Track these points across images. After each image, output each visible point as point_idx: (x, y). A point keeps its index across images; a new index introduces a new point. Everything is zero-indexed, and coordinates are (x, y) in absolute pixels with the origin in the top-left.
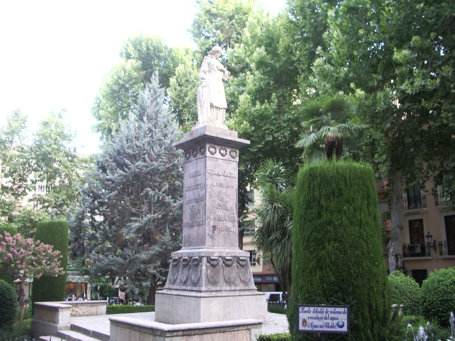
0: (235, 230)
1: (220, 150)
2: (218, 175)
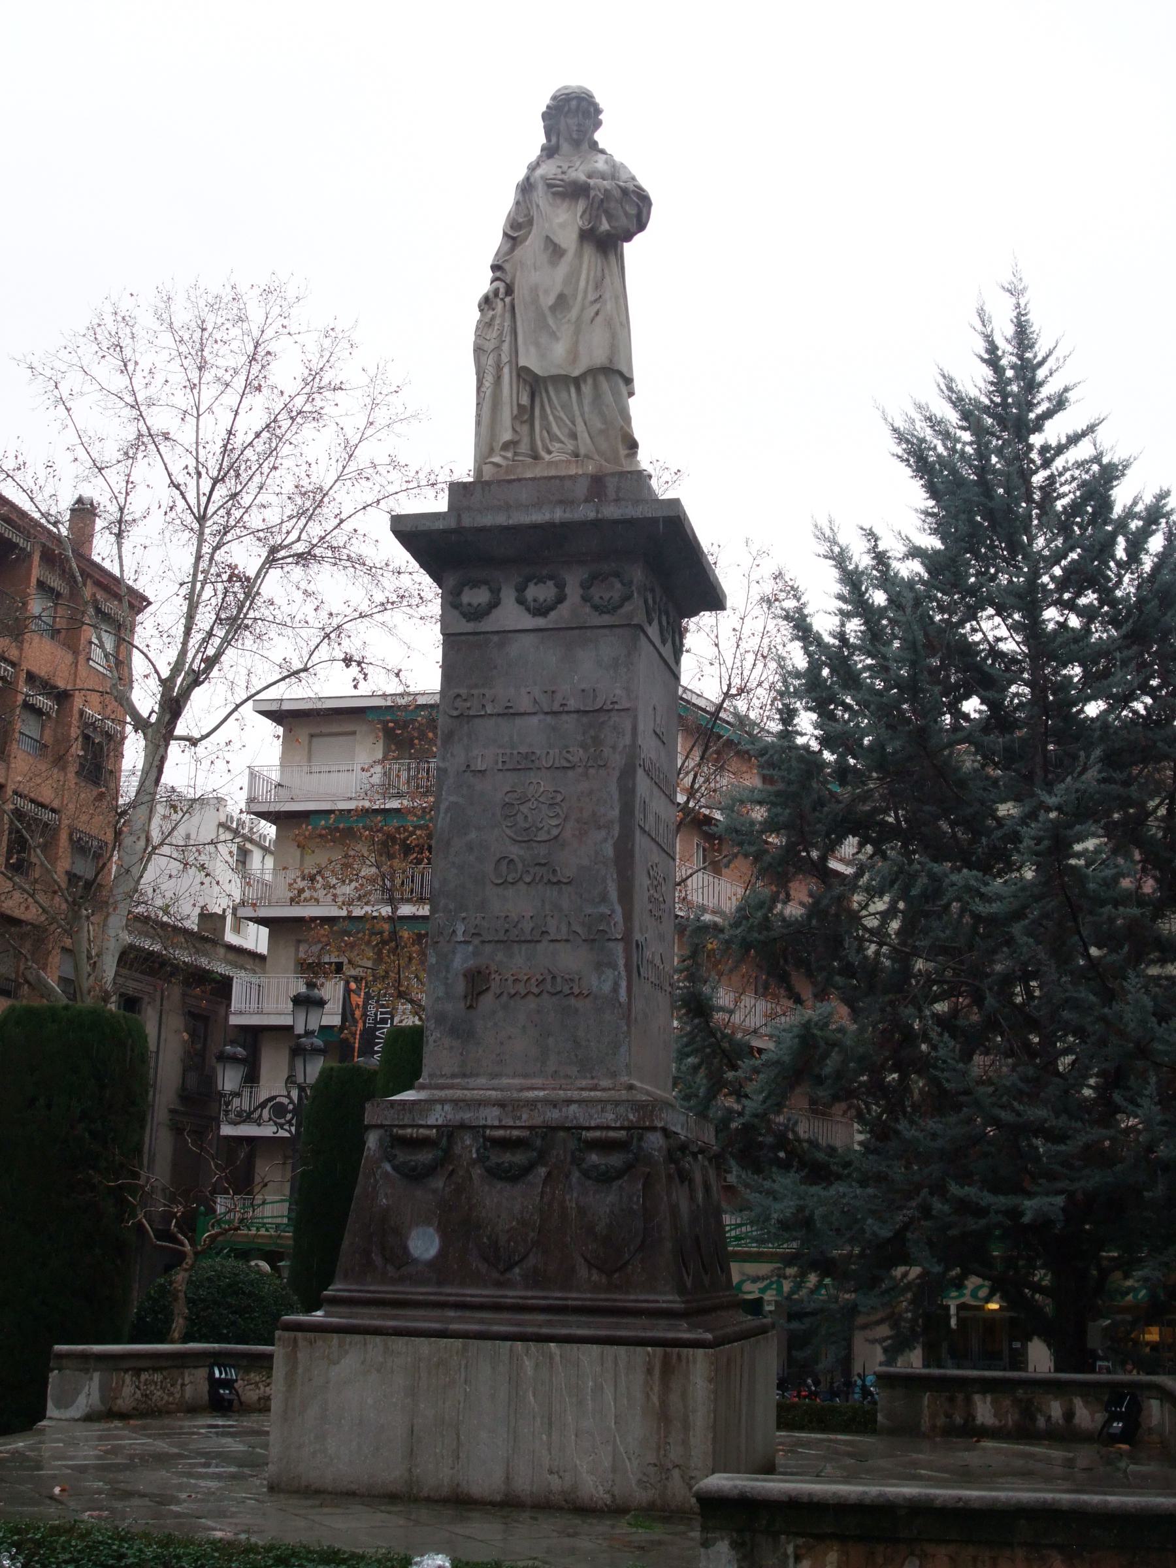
0: (607, 987)
1: (521, 589)
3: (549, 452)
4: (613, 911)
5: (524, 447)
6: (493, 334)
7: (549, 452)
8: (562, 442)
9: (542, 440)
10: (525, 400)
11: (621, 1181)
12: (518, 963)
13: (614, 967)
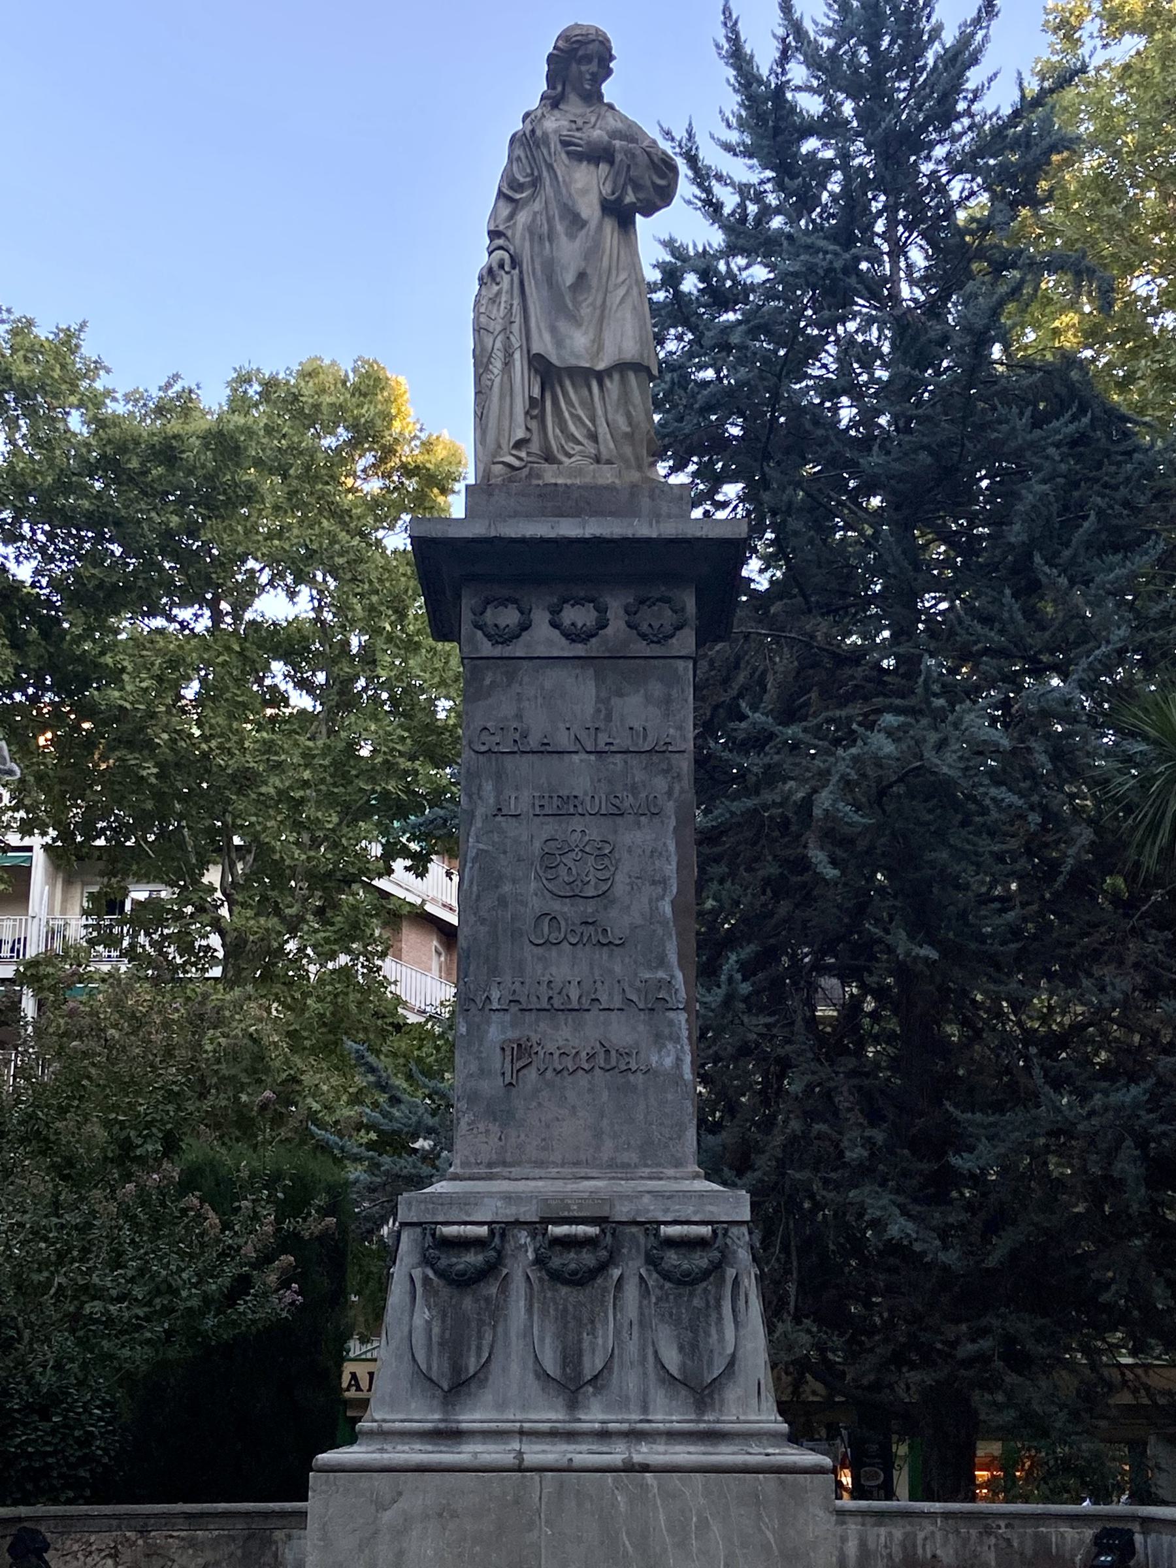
0: (668, 1062)
1: (555, 611)
2: (546, 750)
3: (570, 456)
4: (672, 977)
5: (535, 447)
6: (499, 312)
7: (570, 456)
8: (580, 443)
9: (556, 437)
10: (536, 393)
11: (704, 1284)
12: (559, 1036)
13: (677, 1040)
